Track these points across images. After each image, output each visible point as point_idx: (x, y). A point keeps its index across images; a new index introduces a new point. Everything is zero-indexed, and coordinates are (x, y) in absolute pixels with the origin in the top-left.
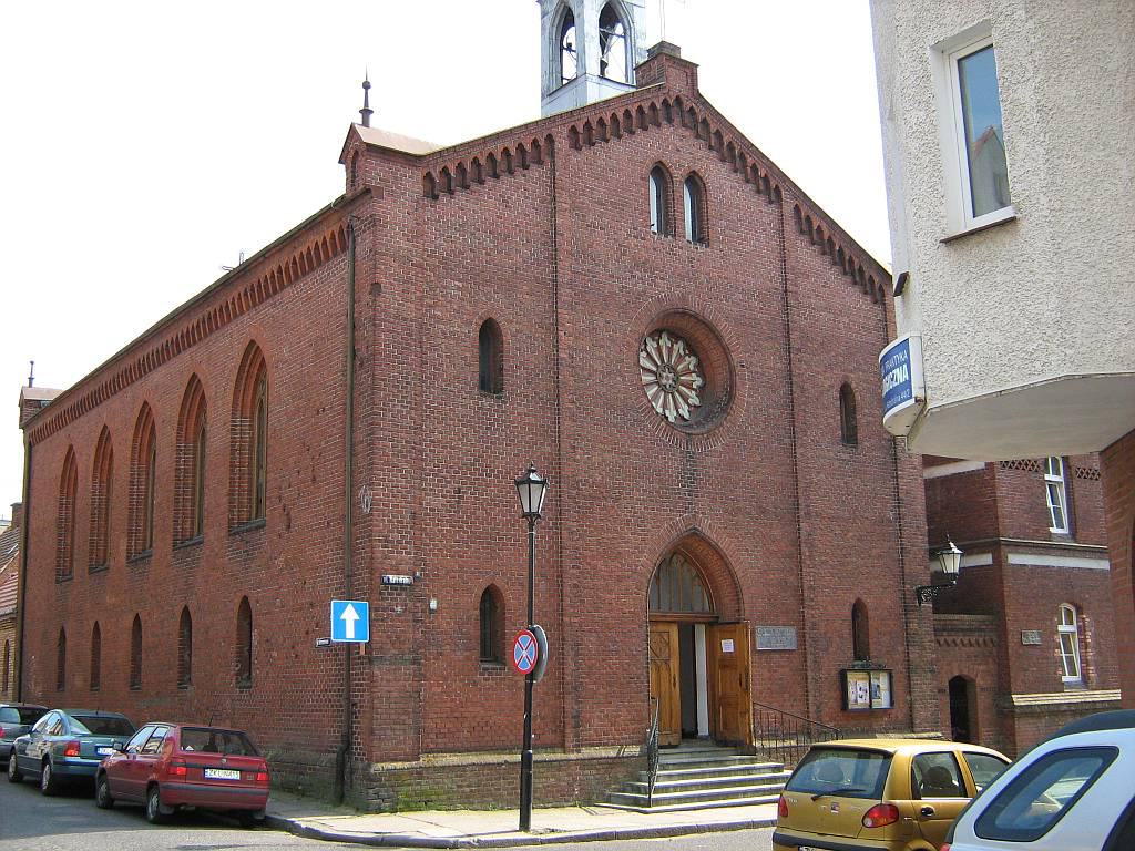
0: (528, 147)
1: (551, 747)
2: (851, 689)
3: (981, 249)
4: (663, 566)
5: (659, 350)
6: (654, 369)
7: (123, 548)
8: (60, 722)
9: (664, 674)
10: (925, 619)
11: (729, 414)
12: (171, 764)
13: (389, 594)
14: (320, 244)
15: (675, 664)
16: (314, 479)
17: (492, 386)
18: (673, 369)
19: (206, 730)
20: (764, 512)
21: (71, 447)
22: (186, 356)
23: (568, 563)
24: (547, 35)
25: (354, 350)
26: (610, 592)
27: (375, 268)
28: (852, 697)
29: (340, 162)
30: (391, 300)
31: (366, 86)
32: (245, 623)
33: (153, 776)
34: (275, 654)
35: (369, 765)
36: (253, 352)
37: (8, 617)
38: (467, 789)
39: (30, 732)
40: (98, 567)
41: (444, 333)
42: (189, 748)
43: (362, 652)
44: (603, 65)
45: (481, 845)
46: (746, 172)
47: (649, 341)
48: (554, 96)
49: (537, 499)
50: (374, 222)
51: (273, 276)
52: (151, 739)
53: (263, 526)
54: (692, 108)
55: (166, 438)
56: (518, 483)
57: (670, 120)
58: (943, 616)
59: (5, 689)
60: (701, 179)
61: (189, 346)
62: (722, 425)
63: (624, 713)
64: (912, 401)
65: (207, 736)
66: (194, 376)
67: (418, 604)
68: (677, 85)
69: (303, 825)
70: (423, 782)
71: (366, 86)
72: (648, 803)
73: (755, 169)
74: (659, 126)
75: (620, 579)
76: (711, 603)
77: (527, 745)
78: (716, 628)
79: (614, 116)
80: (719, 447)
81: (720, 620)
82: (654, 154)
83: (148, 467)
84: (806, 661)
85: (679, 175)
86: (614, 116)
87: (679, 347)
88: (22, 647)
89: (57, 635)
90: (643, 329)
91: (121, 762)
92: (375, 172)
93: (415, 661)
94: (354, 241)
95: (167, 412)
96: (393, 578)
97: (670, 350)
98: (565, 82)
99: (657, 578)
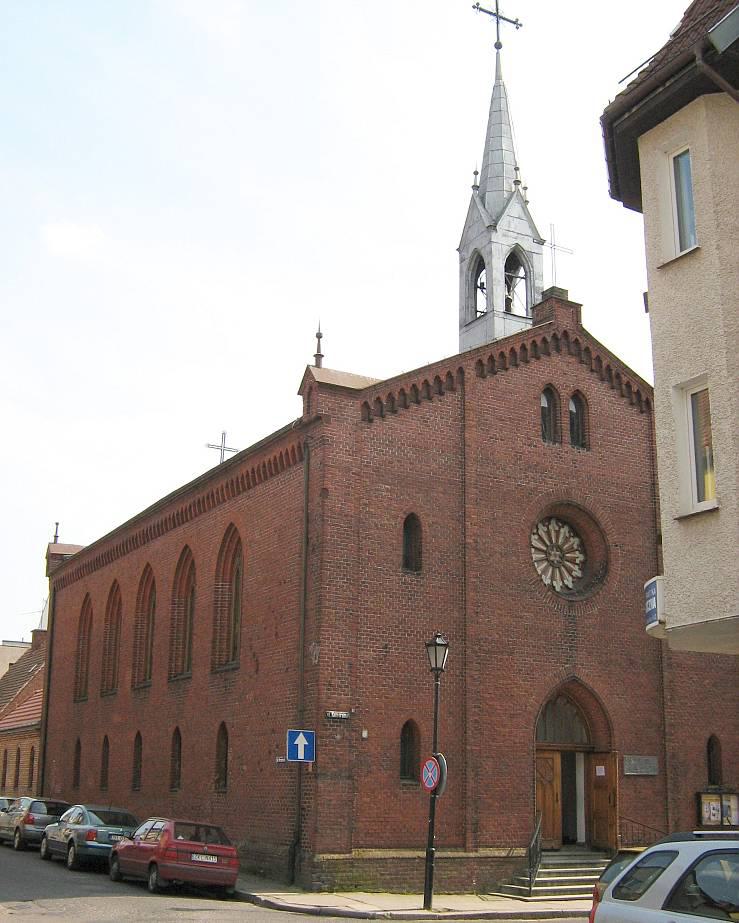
0: (443, 378)
1: (455, 847)
2: (705, 808)
3: (698, 527)
4: (550, 705)
5: (548, 533)
6: (545, 549)
7: (129, 678)
8: (81, 814)
9: (549, 792)
11: (604, 584)
12: (167, 849)
13: (331, 726)
14: (283, 454)
15: (558, 783)
16: (276, 634)
17: (414, 565)
18: (559, 548)
19: (193, 825)
20: (632, 663)
21: (87, 595)
22: (180, 530)
23: (470, 704)
25: (307, 538)
26: (504, 726)
27: (324, 477)
28: (705, 815)
30: (335, 501)
31: (319, 336)
32: (223, 743)
33: (153, 858)
34: (245, 768)
35: (314, 856)
36: (231, 531)
37: (33, 728)
38: (388, 877)
39: (59, 822)
40: (108, 690)
41: (376, 525)
42: (180, 838)
43: (310, 770)
44: (508, 302)
45: (394, 917)
46: (621, 389)
47: (540, 526)
48: (470, 326)
49: (442, 658)
50: (323, 441)
51: (248, 475)
52: (152, 830)
53: (237, 669)
54: (577, 340)
55: (164, 594)
56: (428, 645)
57: (558, 350)
59: (31, 786)
60: (584, 396)
61: (183, 523)
62: (598, 593)
63: (514, 821)
64: (657, 623)
65: (193, 829)
66: (186, 547)
67: (353, 734)
68: (565, 322)
69: (263, 899)
70: (354, 870)
71: (319, 336)
72: (529, 893)
73: (628, 385)
74: (549, 355)
75: (512, 716)
76: (588, 736)
77: (431, 844)
78: (592, 756)
79: (512, 350)
80: (595, 610)
81: (595, 750)
82: (545, 378)
83: (149, 615)
84: (666, 784)
85: (565, 393)
86: (512, 350)
87: (564, 531)
88: (44, 752)
89: (72, 745)
90: (534, 518)
91: (128, 847)
92: (325, 404)
93: (350, 777)
94: (309, 454)
95: (165, 573)
96: (334, 714)
97: (558, 533)
98: (479, 314)
99: (544, 714)
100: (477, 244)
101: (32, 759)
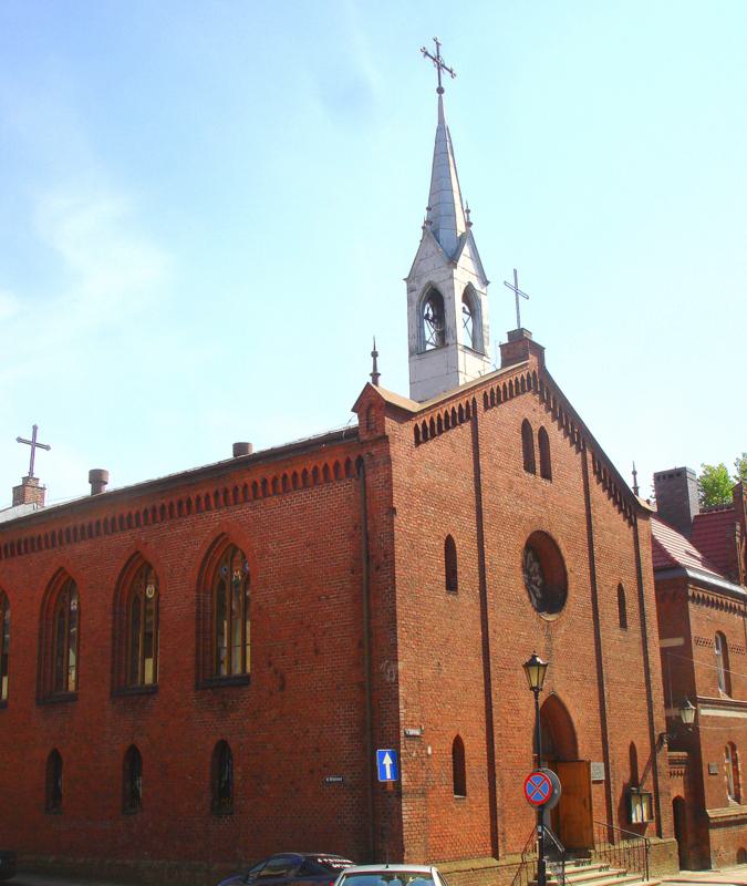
10: (664, 755)
24: (415, 307)
25: (368, 557)
29: (354, 410)
31: (375, 355)
48: (423, 356)
58: (675, 754)
71: (375, 355)
96: (412, 732)
100: (434, 278)
101: (610, 819)
